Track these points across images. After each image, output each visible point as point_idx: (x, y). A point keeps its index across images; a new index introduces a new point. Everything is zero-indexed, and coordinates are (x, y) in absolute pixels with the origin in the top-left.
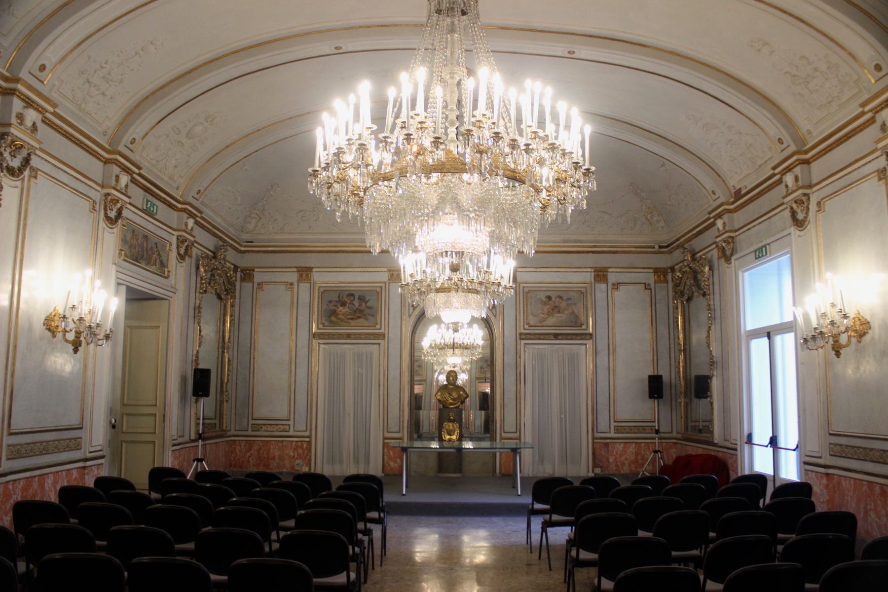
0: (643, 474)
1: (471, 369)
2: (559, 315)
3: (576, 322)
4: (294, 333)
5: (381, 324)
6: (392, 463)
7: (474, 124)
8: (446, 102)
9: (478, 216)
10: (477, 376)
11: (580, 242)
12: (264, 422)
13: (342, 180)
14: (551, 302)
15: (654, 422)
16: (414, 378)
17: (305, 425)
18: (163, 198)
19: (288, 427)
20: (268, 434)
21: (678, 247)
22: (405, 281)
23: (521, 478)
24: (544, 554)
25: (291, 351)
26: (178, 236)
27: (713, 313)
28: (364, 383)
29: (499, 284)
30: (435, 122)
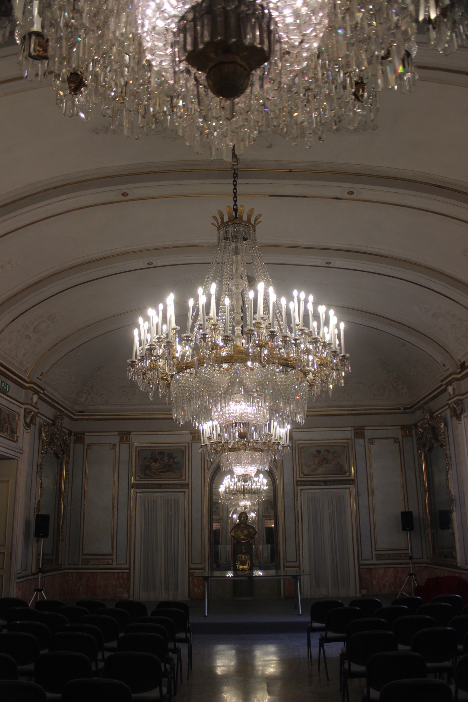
0: (401, 593)
1: (259, 509)
2: (327, 465)
3: (341, 470)
4: (116, 484)
6: (196, 590)
7: (254, 325)
8: (233, 306)
9: (260, 395)
10: (264, 514)
12: (92, 557)
13: (154, 369)
14: (320, 455)
15: (408, 550)
16: (212, 516)
18: (14, 379)
19: (111, 560)
20: (95, 566)
21: (419, 408)
22: (204, 442)
23: (301, 599)
24: (322, 666)
26: (25, 409)
27: (449, 460)
28: (173, 523)
29: (278, 444)
30: (225, 324)
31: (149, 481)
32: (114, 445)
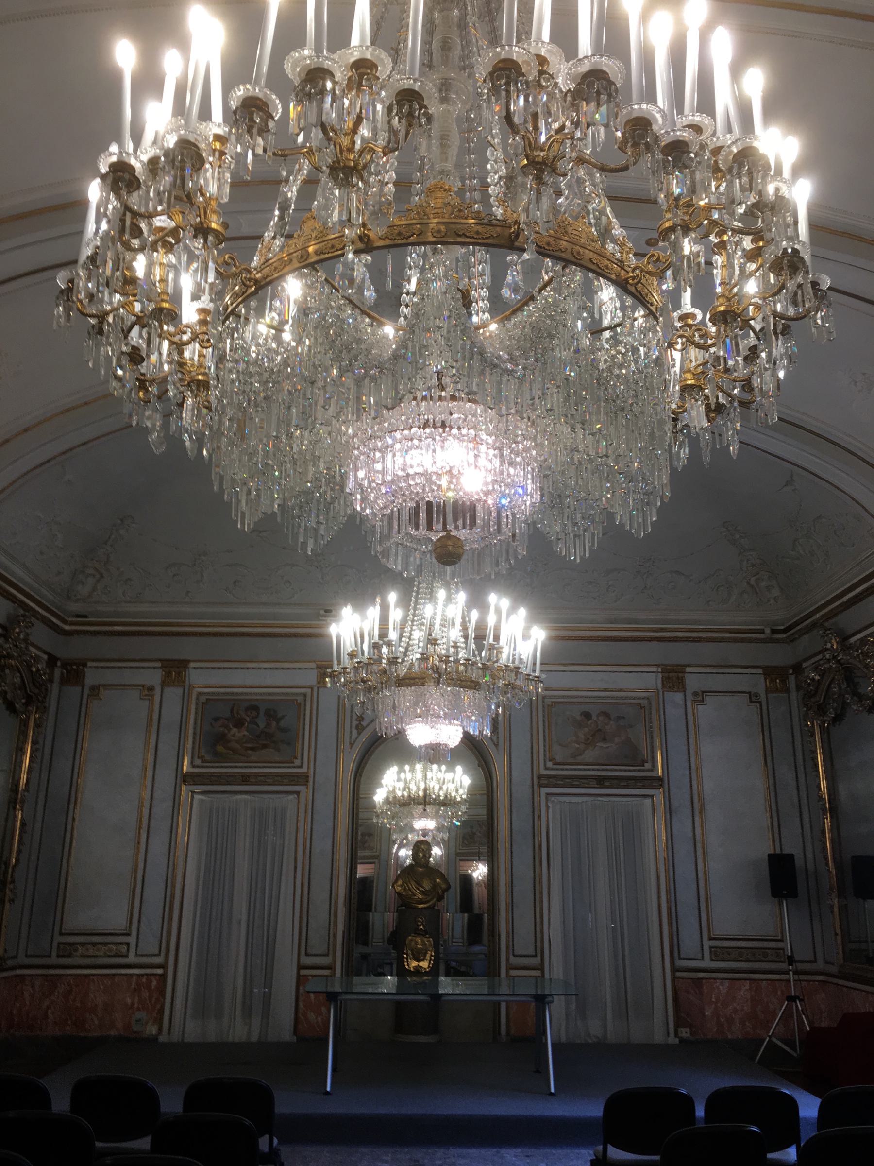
4: (149, 774)
5: (302, 759)
6: (312, 1016)
11: (637, 622)
16: (356, 853)
17: (157, 943)
19: (126, 947)
20: (87, 961)
25: (143, 806)
31: (222, 767)
32: (151, 689)
